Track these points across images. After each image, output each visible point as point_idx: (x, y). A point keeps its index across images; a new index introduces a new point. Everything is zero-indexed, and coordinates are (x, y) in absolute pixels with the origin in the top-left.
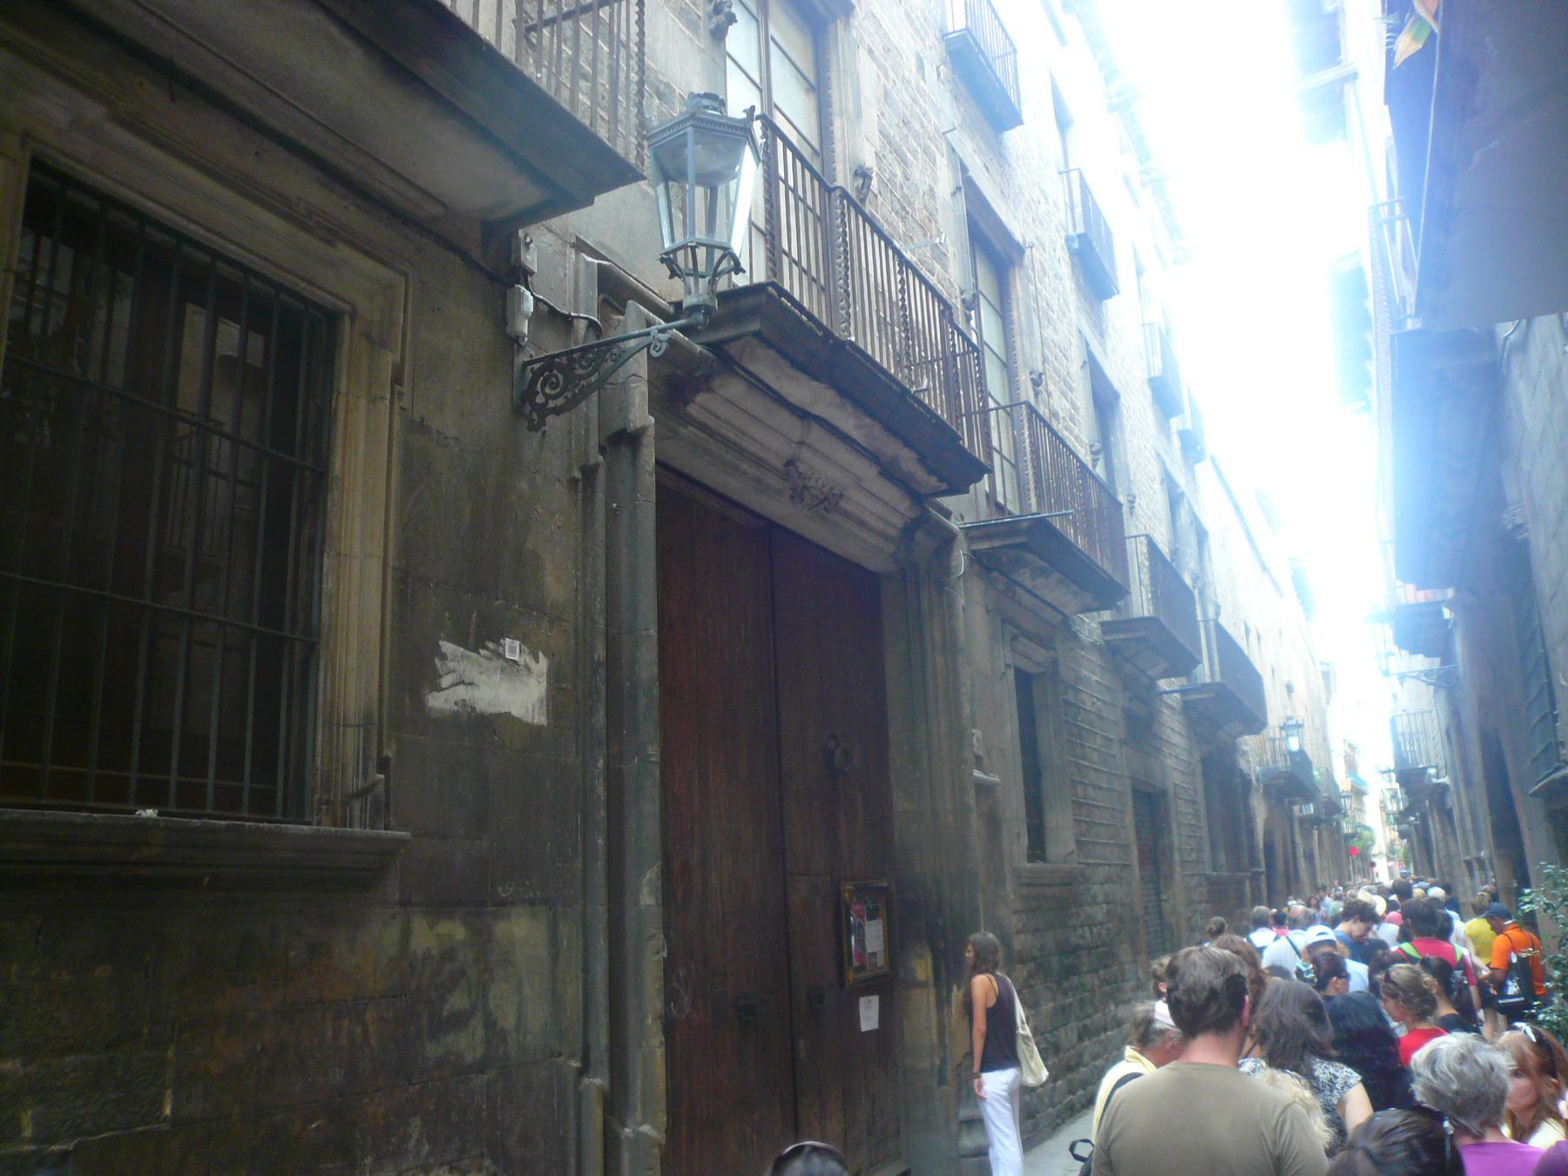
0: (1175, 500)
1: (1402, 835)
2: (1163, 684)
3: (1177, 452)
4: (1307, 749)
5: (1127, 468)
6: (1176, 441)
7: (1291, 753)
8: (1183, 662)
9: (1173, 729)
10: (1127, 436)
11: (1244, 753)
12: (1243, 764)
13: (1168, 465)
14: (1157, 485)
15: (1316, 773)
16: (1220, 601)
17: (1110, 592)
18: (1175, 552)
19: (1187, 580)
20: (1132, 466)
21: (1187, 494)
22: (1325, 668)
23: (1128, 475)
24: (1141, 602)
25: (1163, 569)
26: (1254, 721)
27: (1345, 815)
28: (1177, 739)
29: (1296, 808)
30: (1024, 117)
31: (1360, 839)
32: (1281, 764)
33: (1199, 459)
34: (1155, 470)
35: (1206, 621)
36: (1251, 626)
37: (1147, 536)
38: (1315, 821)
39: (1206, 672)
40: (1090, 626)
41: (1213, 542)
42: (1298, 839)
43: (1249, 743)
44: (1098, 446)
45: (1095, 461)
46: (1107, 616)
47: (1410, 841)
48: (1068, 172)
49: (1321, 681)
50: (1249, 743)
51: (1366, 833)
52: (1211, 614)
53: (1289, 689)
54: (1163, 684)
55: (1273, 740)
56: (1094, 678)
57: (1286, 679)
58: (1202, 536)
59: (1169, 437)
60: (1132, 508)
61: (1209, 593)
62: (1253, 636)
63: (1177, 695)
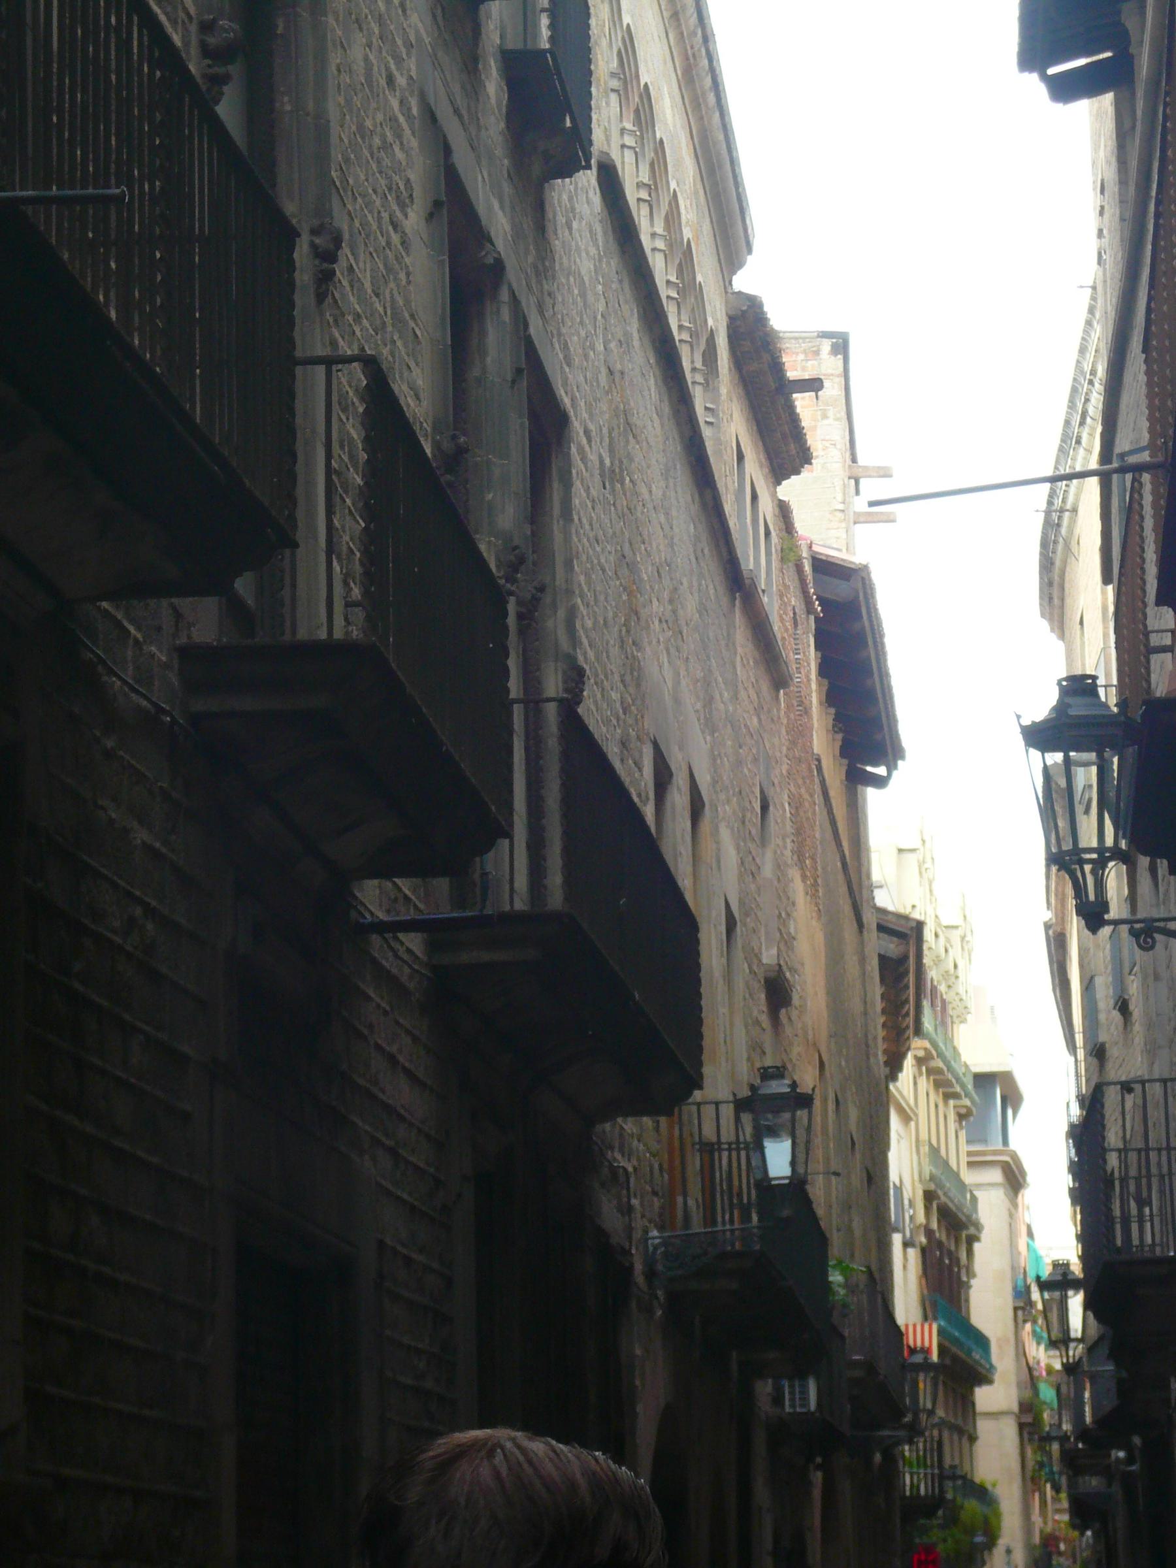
0: (473, 282)
1: (1083, 1512)
2: (373, 898)
3: (494, 127)
4: (817, 1190)
5: (322, 132)
6: (494, 86)
7: (764, 1185)
8: (448, 825)
9: (393, 1061)
10: (334, 28)
11: (617, 1178)
12: (609, 1217)
13: (462, 159)
14: (414, 220)
15: (836, 1277)
16: (586, 657)
17: (231, 525)
18: (456, 458)
19: (488, 549)
20: (340, 135)
21: (512, 273)
22: (892, 948)
23: (322, 159)
24: (326, 594)
25: (416, 491)
26: (658, 1057)
27: (914, 1431)
28: (400, 1093)
29: (764, 1388)
30: (865, 563)
31: (953, 1519)
32: (727, 1224)
33: (568, 166)
34: (413, 164)
35: (533, 701)
36: (676, 760)
37: (371, 364)
38: (816, 1438)
39: (514, 873)
40: (150, 646)
41: (587, 452)
42: (762, 1493)
43: (635, 1141)
44: (229, 28)
45: (218, 81)
46: (204, 621)
47: (1105, 1537)
48: (1147, 1149)
49: (876, 990)
50: (635, 1141)
51: (971, 1506)
52: (553, 685)
53: (778, 992)
54: (373, 898)
55: (709, 1149)
56: (141, 835)
57: (769, 956)
58: (548, 425)
59: (471, 65)
60: (325, 278)
61: (554, 624)
62: (678, 798)
63: (413, 942)
